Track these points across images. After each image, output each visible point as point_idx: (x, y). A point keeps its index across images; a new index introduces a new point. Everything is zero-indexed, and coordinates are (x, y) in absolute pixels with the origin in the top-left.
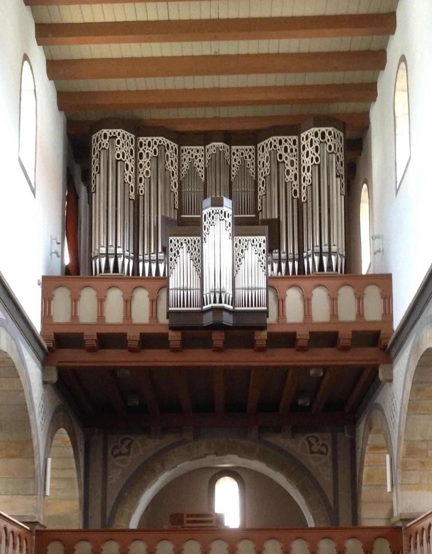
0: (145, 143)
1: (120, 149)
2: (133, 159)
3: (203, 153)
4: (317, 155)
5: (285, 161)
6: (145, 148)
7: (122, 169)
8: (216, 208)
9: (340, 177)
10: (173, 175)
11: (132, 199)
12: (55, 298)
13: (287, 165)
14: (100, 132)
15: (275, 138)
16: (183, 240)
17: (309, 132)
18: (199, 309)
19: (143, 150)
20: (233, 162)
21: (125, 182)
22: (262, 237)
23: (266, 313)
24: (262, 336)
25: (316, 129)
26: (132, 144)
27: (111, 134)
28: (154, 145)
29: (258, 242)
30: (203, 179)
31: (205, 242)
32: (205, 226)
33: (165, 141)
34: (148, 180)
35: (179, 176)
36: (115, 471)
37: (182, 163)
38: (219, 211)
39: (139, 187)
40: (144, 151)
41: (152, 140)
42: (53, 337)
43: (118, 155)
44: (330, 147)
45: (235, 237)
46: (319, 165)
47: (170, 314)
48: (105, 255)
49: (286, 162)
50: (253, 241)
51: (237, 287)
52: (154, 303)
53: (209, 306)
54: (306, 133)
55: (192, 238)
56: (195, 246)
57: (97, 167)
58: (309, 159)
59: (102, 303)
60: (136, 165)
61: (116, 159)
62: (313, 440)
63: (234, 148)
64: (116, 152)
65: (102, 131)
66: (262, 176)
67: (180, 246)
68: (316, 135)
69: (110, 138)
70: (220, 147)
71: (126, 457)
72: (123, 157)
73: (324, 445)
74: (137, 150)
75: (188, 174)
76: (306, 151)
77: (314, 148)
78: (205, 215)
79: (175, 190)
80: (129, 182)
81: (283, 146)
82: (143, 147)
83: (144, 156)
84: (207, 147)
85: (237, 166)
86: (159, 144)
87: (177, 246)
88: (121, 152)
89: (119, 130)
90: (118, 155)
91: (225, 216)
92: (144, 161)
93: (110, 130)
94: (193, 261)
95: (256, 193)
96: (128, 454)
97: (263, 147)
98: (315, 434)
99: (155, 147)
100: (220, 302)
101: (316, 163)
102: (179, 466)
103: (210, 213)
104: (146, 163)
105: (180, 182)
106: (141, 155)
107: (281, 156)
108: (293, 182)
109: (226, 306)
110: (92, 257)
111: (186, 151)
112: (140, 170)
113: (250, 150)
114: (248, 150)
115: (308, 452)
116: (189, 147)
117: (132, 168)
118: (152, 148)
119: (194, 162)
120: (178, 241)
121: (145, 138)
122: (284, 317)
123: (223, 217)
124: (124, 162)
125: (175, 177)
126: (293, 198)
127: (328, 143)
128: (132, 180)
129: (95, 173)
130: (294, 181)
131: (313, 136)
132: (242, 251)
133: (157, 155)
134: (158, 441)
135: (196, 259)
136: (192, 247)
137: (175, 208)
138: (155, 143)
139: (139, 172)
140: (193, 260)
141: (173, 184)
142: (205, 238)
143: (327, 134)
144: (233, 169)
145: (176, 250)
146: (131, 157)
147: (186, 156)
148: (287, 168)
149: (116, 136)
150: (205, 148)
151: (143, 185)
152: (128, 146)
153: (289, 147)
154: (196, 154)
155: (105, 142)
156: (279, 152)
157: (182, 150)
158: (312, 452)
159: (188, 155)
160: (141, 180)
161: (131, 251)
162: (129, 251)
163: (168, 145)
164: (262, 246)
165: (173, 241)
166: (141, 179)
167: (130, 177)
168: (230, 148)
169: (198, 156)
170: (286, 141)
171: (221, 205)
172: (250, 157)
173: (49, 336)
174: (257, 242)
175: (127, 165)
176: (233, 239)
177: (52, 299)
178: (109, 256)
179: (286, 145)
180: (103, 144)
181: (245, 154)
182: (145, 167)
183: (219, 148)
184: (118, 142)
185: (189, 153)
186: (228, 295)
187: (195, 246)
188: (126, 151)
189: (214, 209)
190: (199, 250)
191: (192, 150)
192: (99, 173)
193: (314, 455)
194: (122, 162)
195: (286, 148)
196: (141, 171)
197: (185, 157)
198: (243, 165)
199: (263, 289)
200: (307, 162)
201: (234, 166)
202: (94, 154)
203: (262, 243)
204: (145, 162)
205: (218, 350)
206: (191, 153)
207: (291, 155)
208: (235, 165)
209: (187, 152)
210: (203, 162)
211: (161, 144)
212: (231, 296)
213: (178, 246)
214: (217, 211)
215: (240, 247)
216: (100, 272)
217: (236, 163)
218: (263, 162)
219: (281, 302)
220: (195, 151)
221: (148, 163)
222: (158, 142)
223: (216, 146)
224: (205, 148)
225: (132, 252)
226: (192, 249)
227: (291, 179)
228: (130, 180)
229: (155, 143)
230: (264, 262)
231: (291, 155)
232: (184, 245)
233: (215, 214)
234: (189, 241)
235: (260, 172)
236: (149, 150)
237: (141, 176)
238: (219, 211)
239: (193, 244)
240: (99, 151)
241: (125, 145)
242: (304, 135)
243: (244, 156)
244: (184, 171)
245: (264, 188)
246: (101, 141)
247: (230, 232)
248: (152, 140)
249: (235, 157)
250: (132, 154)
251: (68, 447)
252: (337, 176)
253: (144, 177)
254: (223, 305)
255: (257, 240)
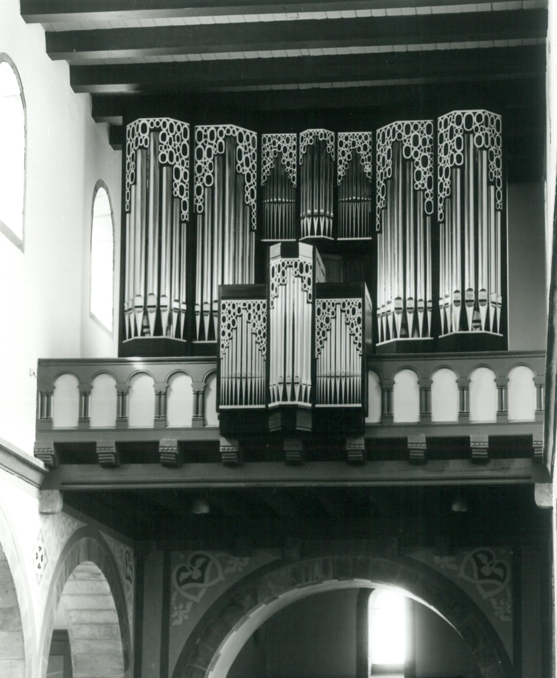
0: (205, 134)
1: (165, 147)
2: (186, 159)
3: (295, 143)
4: (459, 152)
5: (414, 157)
6: (206, 142)
7: (170, 179)
8: (288, 259)
9: (494, 185)
10: (249, 180)
11: (185, 221)
12: (57, 392)
13: (417, 164)
14: (137, 121)
15: (400, 122)
16: (242, 304)
17: (448, 116)
18: (263, 406)
19: (203, 144)
20: (339, 156)
21: (173, 197)
22: (356, 299)
23: (364, 412)
24: (357, 445)
25: (459, 112)
26: (185, 137)
27: (152, 124)
28: (219, 137)
29: (351, 307)
30: (295, 183)
31: (273, 308)
32: (273, 285)
33: (235, 129)
34: (210, 190)
35: (259, 181)
36: (181, 606)
37: (264, 159)
38: (292, 263)
39: (197, 201)
40: (205, 147)
41: (217, 128)
42: (53, 449)
43: (163, 158)
44: (479, 140)
45: (316, 300)
46: (462, 168)
47: (223, 415)
48: (142, 309)
49: (417, 159)
50: (344, 305)
51: (318, 373)
52: (200, 396)
53: (277, 403)
54: (445, 116)
55: (254, 301)
56: (260, 313)
57: (132, 174)
58: (447, 158)
59: (125, 396)
60: (191, 169)
61: (160, 163)
62: (483, 558)
63: (342, 135)
64: (159, 152)
65: (140, 121)
66: (382, 180)
67: (237, 313)
68: (459, 120)
69: (151, 130)
70: (319, 134)
71: (198, 585)
72: (171, 159)
73: (500, 565)
74: (192, 143)
75: (275, 169)
76: (444, 144)
77: (455, 141)
78: (273, 268)
79: (252, 201)
80: (180, 196)
81: (412, 135)
82: (203, 140)
83: (205, 153)
84: (302, 134)
85: (346, 163)
86: (226, 136)
87: (232, 314)
88: (167, 152)
89: (164, 119)
90: (163, 158)
91: (301, 271)
92: (204, 161)
93: (151, 120)
94: (256, 336)
95: (374, 205)
96: (201, 580)
97: (384, 133)
98: (487, 549)
99: (221, 140)
100: (293, 398)
101: (457, 164)
102: (281, 597)
103: (279, 265)
104: (208, 164)
105: (259, 187)
106: (200, 152)
107: (408, 150)
108: (425, 190)
109: (302, 403)
110: (126, 309)
111: (269, 140)
112: (198, 175)
113: (366, 138)
114: (363, 137)
115: (476, 575)
116: (274, 135)
117: (185, 174)
118: (216, 142)
119: (282, 158)
120: (234, 307)
121: (205, 127)
122: (391, 417)
123: (298, 273)
124: (172, 166)
125: (252, 182)
126: (425, 216)
127: (477, 134)
128: (185, 192)
129: (131, 183)
130: (427, 188)
131: (453, 122)
132: (327, 320)
133: (223, 152)
134: (246, 560)
135: (260, 332)
136: (254, 314)
137: (251, 230)
138: (221, 133)
139: (197, 179)
140: (256, 334)
141: (248, 194)
142: (272, 302)
143: (474, 119)
144: (340, 167)
145: (231, 319)
146: (184, 157)
147: (269, 147)
148: (418, 168)
149: (160, 127)
150: (298, 136)
151: (203, 198)
152: (178, 141)
153: (421, 136)
154: (285, 145)
155: (144, 137)
156: (406, 145)
157: (265, 139)
158: (481, 576)
159: (273, 146)
160: (199, 190)
161: (183, 299)
162: (178, 301)
163: (240, 134)
164: (356, 312)
165: (227, 306)
166: (199, 189)
167: (181, 188)
168: (336, 135)
169: (288, 148)
170: (416, 127)
171: (295, 254)
172: (365, 148)
173: (46, 449)
174: (349, 308)
175: (177, 171)
176: (313, 304)
177: (52, 393)
178: (149, 309)
179: (416, 133)
180: (141, 140)
181: (358, 143)
182: (206, 170)
183: (318, 136)
184: (164, 137)
185: (274, 143)
186: (304, 387)
187: (260, 313)
188: (175, 150)
189: (285, 260)
190: (264, 318)
191: (279, 139)
192: (135, 183)
193: (486, 581)
194: (169, 168)
195: (416, 138)
196: (200, 176)
197: (268, 149)
198: (355, 158)
199: (357, 376)
200: (445, 161)
201: (341, 161)
202: (129, 154)
203: (357, 308)
204: (205, 163)
205: (293, 464)
206: (278, 143)
207: (423, 148)
208: (343, 161)
209: (272, 141)
210: (295, 158)
211: (230, 134)
212: (309, 388)
213: (234, 314)
214: (290, 263)
215: (324, 314)
216: (136, 334)
217: (344, 158)
218: (384, 158)
219: (386, 394)
220: (283, 140)
221: (210, 164)
222: (225, 132)
223: (313, 134)
224: (298, 136)
225: (184, 301)
226: (255, 317)
227: (423, 185)
228: (182, 193)
229: (221, 133)
230: (359, 337)
231: (423, 148)
232: (243, 312)
233: (232, 331)
234: (250, 306)
235: (379, 172)
236: (212, 144)
237: (199, 184)
238: (292, 263)
239: (256, 310)
240: (136, 151)
241: (174, 141)
242: (442, 118)
243: (356, 147)
244: (266, 171)
245: (383, 198)
246: (137, 136)
247: (310, 292)
248: (217, 128)
249: (342, 149)
250: (185, 153)
251: (101, 581)
252: (489, 184)
253: (205, 187)
254: (296, 402)
255: (349, 304)
